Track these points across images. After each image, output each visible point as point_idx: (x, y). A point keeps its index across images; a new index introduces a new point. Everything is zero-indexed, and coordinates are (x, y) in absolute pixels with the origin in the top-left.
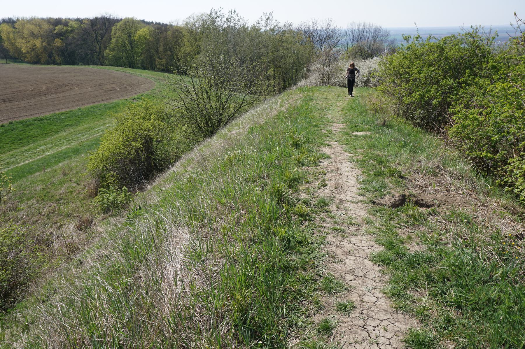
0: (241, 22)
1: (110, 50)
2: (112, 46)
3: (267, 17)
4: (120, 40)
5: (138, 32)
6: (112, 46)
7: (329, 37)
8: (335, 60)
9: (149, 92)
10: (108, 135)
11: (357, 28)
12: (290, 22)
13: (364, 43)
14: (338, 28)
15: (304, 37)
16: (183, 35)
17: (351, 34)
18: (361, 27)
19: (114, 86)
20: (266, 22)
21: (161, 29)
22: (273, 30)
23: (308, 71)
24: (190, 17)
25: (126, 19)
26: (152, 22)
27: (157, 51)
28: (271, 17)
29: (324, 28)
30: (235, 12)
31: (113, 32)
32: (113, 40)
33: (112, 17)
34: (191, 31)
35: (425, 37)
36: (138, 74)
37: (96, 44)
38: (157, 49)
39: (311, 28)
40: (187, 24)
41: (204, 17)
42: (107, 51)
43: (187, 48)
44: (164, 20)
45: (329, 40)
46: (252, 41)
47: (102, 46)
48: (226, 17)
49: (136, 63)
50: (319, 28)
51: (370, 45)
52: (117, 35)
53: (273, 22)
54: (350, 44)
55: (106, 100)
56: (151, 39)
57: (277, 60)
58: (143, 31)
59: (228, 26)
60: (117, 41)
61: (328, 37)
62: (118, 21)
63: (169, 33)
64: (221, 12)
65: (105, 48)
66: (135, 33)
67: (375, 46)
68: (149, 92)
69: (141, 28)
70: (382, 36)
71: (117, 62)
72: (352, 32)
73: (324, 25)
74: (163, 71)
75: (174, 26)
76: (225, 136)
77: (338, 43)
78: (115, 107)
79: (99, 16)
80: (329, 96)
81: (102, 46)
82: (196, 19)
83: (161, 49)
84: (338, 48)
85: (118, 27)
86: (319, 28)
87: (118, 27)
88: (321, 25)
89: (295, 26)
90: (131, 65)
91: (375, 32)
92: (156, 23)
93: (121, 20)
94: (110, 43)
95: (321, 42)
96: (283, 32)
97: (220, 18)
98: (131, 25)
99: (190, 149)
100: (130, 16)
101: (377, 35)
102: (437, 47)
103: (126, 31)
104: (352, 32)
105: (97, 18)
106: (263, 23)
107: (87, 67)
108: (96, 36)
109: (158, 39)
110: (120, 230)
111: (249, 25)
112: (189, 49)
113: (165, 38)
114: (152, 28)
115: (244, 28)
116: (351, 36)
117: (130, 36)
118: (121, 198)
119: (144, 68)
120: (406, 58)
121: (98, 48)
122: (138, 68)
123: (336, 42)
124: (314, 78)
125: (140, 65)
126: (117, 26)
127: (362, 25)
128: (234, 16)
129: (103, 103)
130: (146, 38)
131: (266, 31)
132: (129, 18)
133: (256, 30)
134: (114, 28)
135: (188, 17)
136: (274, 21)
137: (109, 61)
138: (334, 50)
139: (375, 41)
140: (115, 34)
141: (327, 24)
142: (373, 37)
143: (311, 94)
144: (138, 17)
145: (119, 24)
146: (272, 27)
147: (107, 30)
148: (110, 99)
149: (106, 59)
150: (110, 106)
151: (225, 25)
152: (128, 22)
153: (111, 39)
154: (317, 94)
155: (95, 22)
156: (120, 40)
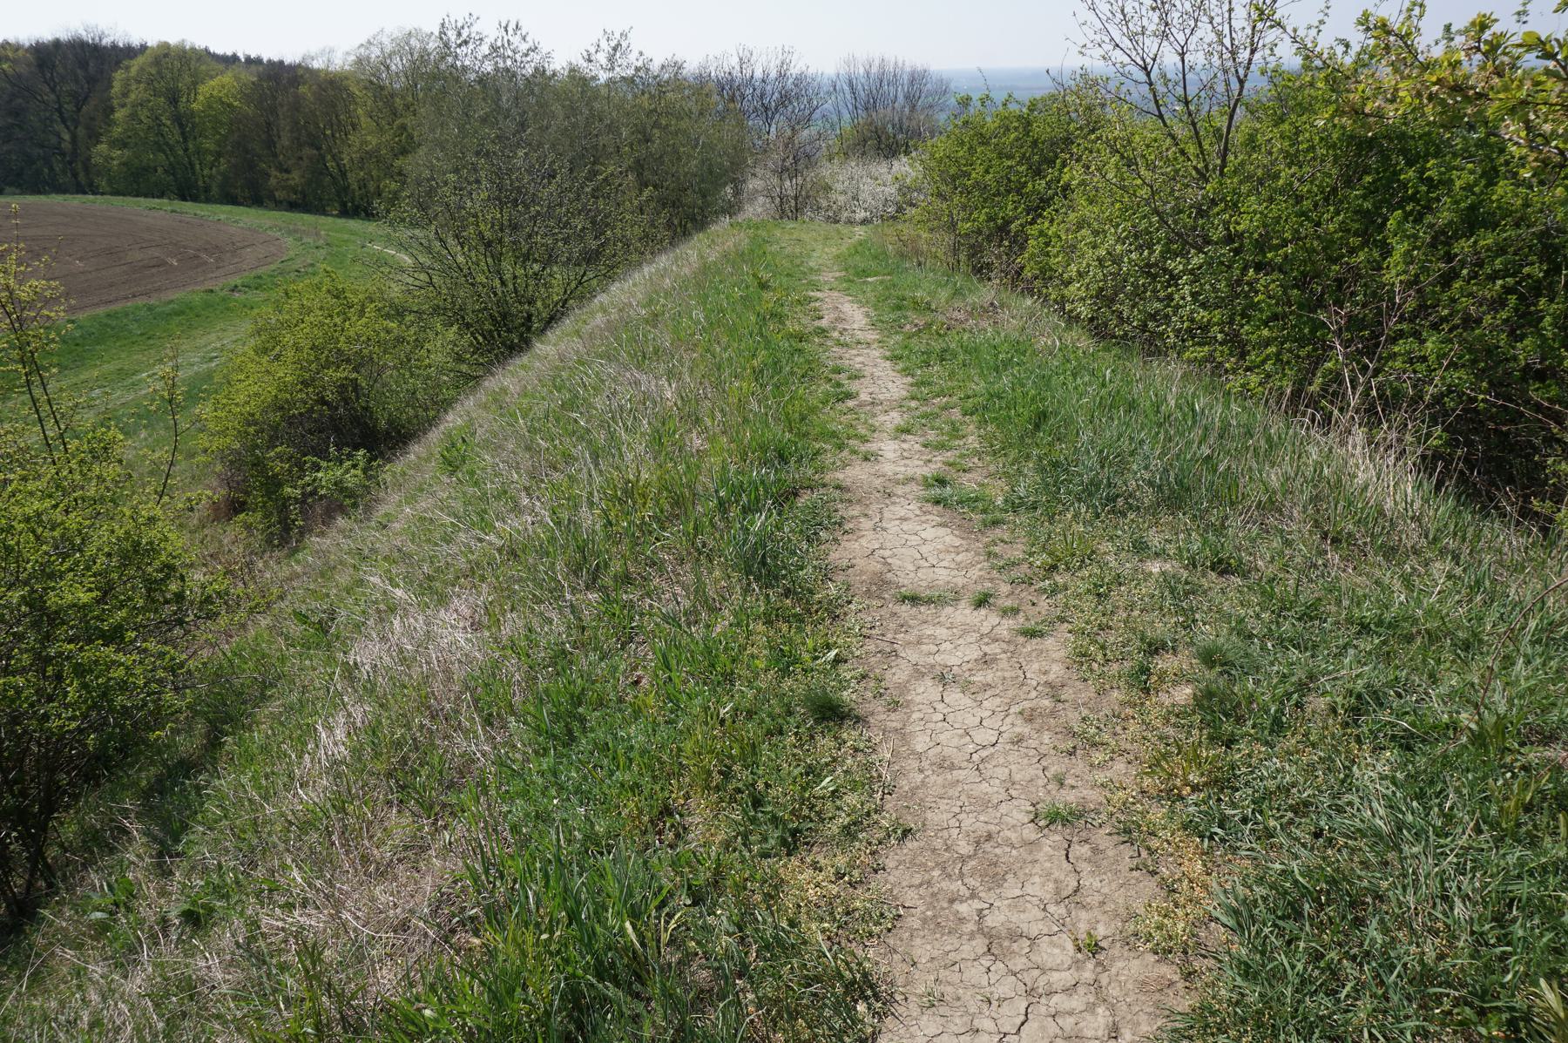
0: (536, 58)
1: (113, 144)
2: (117, 131)
3: (613, 44)
4: (143, 114)
5: (202, 89)
6: (117, 131)
7: (785, 99)
9: (273, 267)
10: (234, 363)
11: (862, 71)
12: (678, 58)
13: (883, 114)
14: (811, 71)
15: (716, 98)
16: (351, 95)
17: (846, 88)
18: (874, 70)
19: (156, 252)
20: (611, 59)
21: (278, 79)
22: (629, 81)
23: (737, 193)
24: (369, 42)
26: (235, 58)
27: (270, 144)
28: (624, 44)
29: (773, 74)
31: (117, 87)
32: (119, 115)
33: (106, 41)
34: (376, 89)
35: (999, 97)
36: (222, 217)
37: (60, 127)
38: (278, 141)
39: (736, 73)
40: (359, 61)
41: (413, 42)
43: (368, 136)
45: (790, 108)
46: (572, 110)
47: (81, 132)
48: (488, 41)
49: (200, 183)
50: (758, 74)
51: (900, 120)
54: (846, 116)
55: (147, 294)
56: (249, 110)
57: (652, 162)
59: (497, 70)
60: (133, 116)
61: (785, 99)
62: (130, 52)
63: (303, 89)
64: (474, 29)
65: (95, 137)
67: (914, 123)
68: (273, 267)
69: (212, 78)
70: (929, 94)
71: (137, 182)
72: (850, 82)
73: (772, 65)
74: (293, 206)
76: (498, 401)
77: (814, 116)
78: (183, 313)
79: (64, 36)
80: (804, 236)
81: (81, 132)
84: (813, 130)
85: (134, 71)
86: (758, 74)
87: (134, 71)
88: (763, 65)
89: (691, 67)
90: (187, 191)
91: (912, 81)
92: (249, 61)
93: (144, 48)
94: (111, 124)
95: (767, 113)
96: (661, 85)
97: (471, 46)
98: (177, 68)
99: (469, 381)
101: (917, 89)
102: (1019, 118)
103: (160, 85)
104: (850, 82)
105: (57, 44)
106: (602, 58)
107: (42, 198)
108: (58, 101)
111: (558, 63)
112: (373, 140)
113: (296, 106)
114: (250, 77)
116: (848, 96)
117: (174, 100)
118: (353, 478)
119: (233, 201)
120: (962, 144)
121: (67, 137)
122: (208, 201)
123: (807, 112)
124: (757, 209)
125: (215, 191)
126: (128, 68)
127: (877, 63)
128: (516, 40)
129: (140, 302)
130: (230, 105)
131: (611, 82)
133: (577, 78)
134: (119, 75)
136: (632, 57)
137: (110, 182)
139: (913, 108)
140: (125, 95)
141: (778, 62)
142: (907, 97)
143: (764, 234)
145: (136, 64)
146: (631, 72)
147: (92, 81)
148: (158, 290)
149: (99, 174)
150: (168, 309)
151: (488, 67)
152: (166, 56)
154: (778, 233)
155: (47, 56)
156: (143, 114)
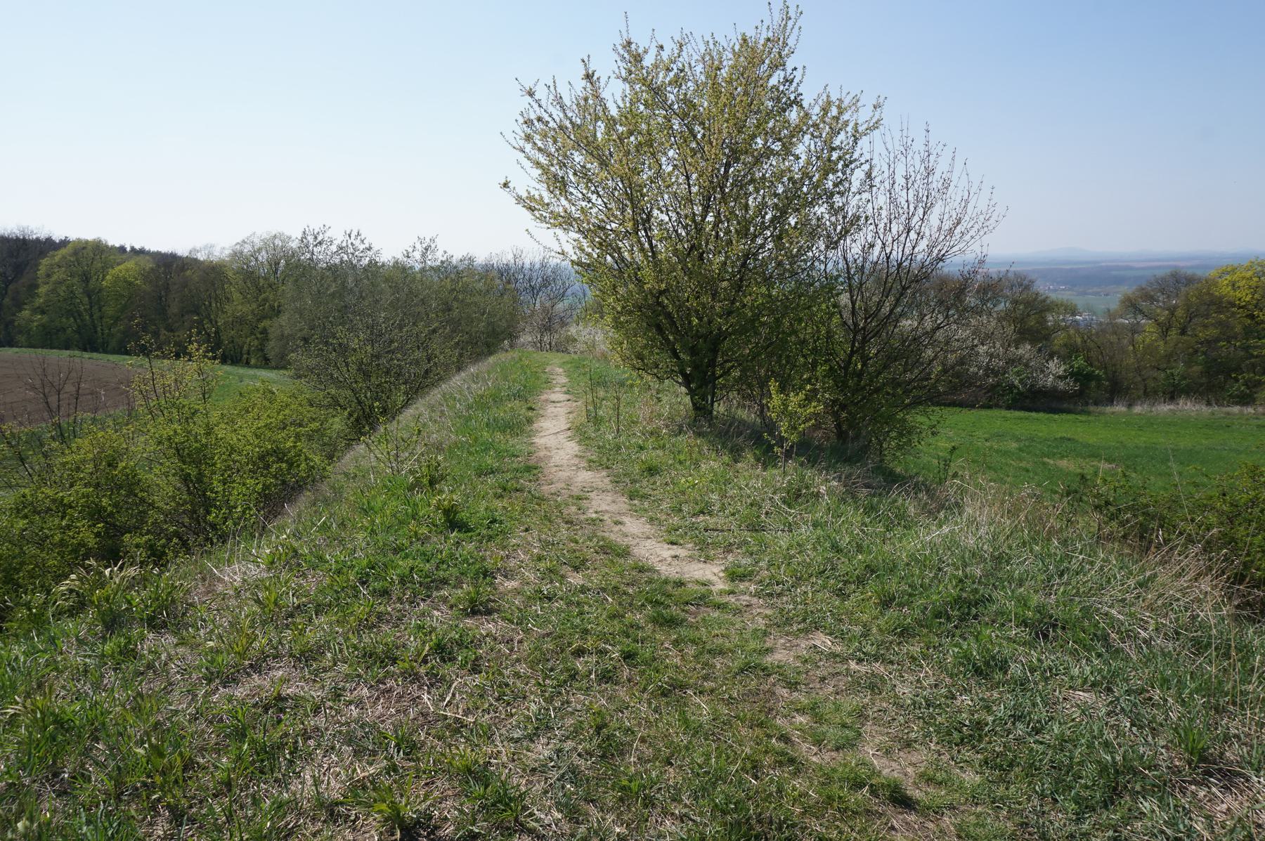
2: (39, 301)
8: (563, 324)
15: (498, 281)
21: (168, 264)
25: (79, 241)
29: (537, 266)
30: (358, 234)
31: (42, 270)
32: (43, 290)
42: (26, 313)
44: (182, 250)
50: (527, 266)
52: (55, 278)
53: (440, 256)
56: (147, 288)
58: (127, 268)
61: (546, 282)
64: (327, 235)
66: (104, 269)
71: (49, 338)
75: (203, 262)
82: (258, 244)
83: (174, 309)
86: (527, 266)
89: (481, 258)
90: (90, 343)
100: (88, 235)
106: (417, 255)
109: (167, 288)
110: (652, 433)
115: (374, 268)
128: (357, 243)
132: (87, 242)
133: (401, 269)
135: (239, 240)
138: (560, 306)
140: (48, 276)
144: (114, 239)
153: (37, 286)
